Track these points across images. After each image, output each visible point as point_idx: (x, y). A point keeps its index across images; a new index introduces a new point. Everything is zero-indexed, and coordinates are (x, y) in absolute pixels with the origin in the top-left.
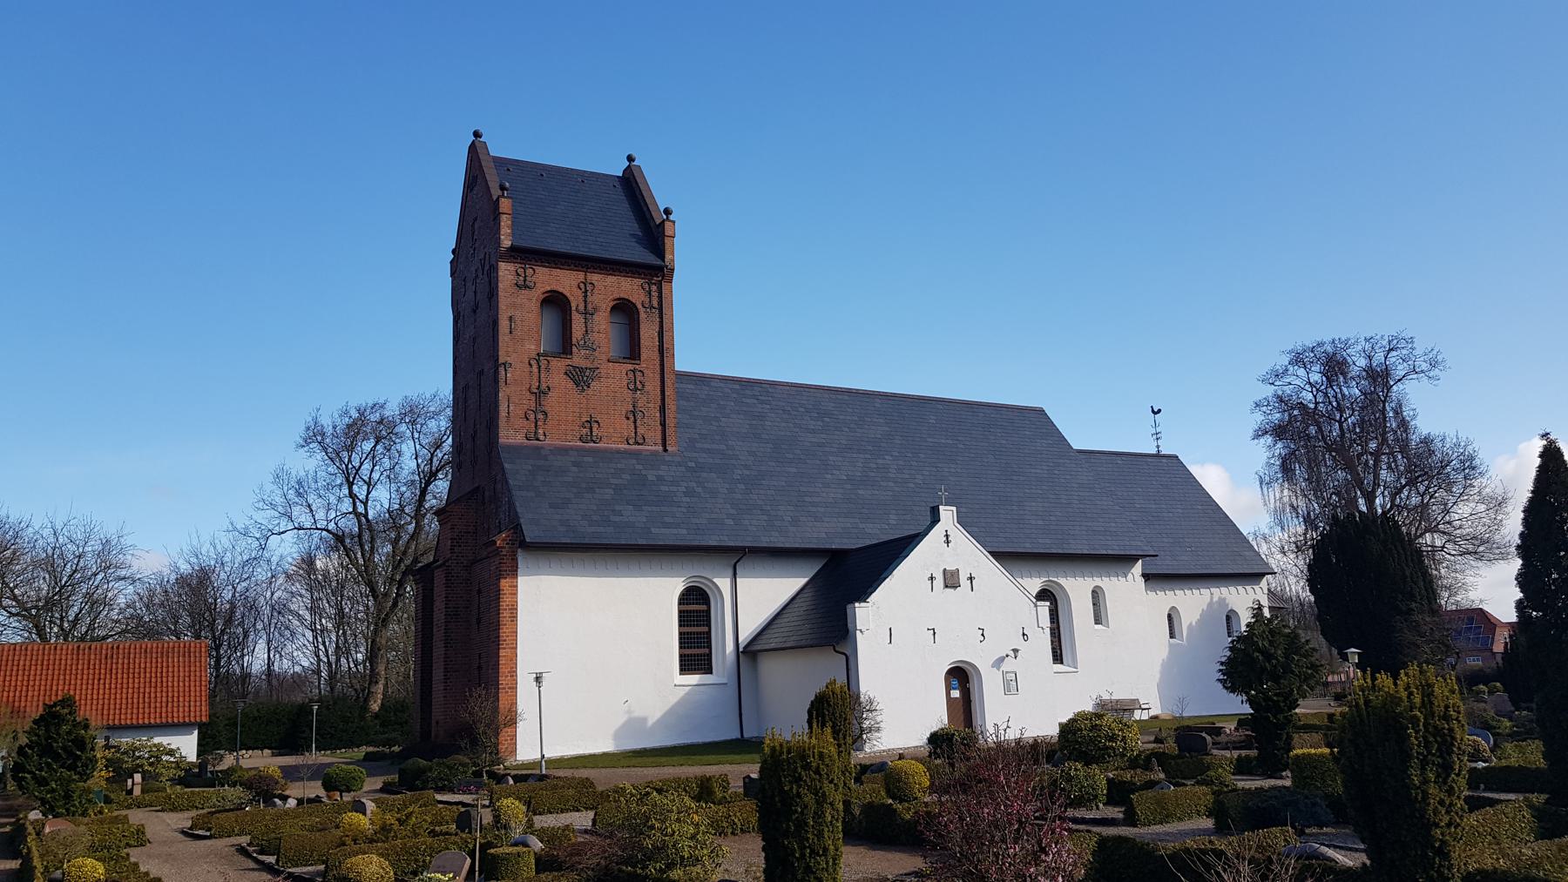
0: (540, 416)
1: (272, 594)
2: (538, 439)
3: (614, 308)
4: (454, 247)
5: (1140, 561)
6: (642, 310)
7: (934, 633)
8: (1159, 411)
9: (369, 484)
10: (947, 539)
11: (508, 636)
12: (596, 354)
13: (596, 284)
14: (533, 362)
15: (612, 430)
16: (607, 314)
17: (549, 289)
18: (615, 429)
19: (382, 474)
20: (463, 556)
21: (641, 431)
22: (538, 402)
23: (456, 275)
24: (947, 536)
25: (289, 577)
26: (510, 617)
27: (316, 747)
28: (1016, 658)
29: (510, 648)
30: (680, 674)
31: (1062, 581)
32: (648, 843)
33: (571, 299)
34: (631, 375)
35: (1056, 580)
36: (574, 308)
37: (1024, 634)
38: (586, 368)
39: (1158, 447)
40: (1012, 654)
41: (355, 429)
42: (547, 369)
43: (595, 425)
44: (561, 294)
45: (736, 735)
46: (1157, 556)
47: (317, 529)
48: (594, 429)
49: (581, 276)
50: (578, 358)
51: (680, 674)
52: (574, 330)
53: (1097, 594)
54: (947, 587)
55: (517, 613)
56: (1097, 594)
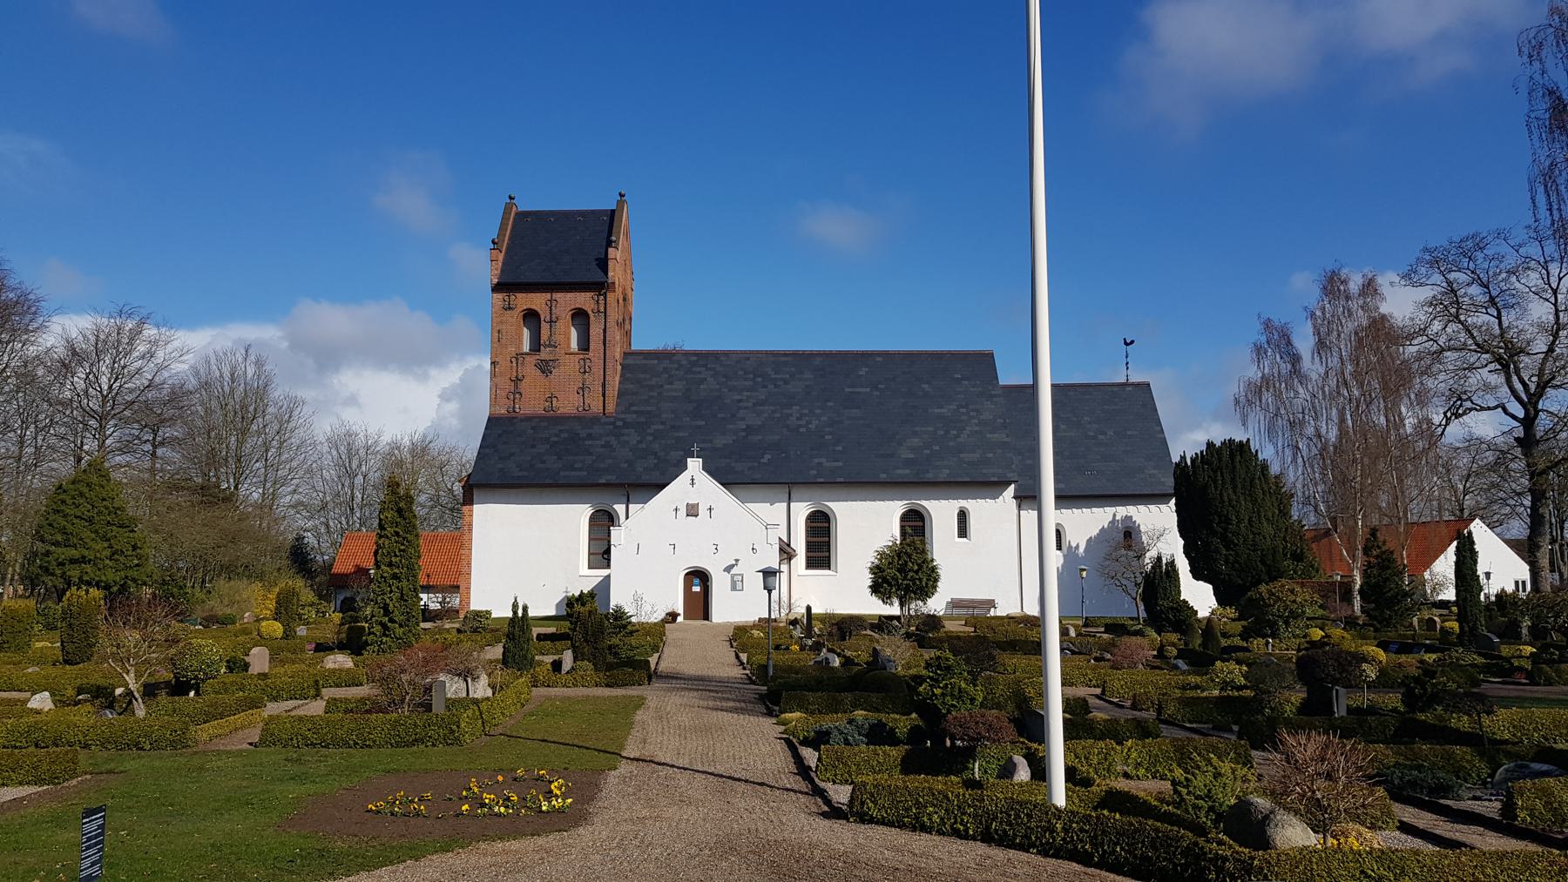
0: (517, 396)
3: (573, 316)
5: (1013, 485)
8: (1132, 342)
13: (558, 300)
14: (513, 360)
18: (569, 401)
22: (516, 386)
24: (693, 480)
31: (924, 503)
33: (540, 312)
34: (582, 362)
35: (918, 502)
36: (542, 319)
37: (753, 549)
42: (523, 364)
43: (554, 399)
44: (534, 310)
49: (548, 296)
50: (545, 354)
53: (963, 516)
54: (688, 515)
56: (963, 516)
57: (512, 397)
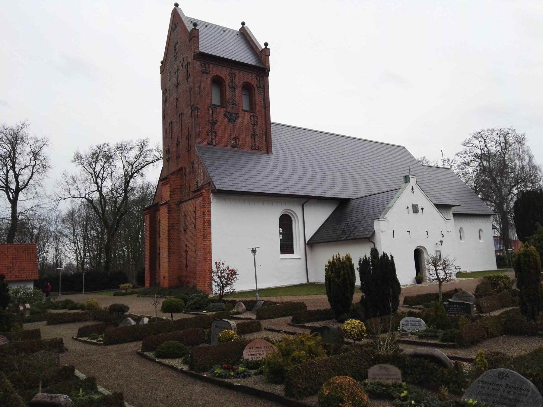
1: (57, 227)
2: (212, 145)
4: (162, 60)
6: (256, 89)
7: (410, 233)
9: (102, 180)
10: (413, 190)
11: (207, 235)
12: (237, 107)
14: (210, 108)
15: (244, 143)
16: (240, 89)
17: (216, 75)
19: (108, 175)
20: (175, 200)
21: (257, 144)
23: (164, 72)
24: (413, 189)
25: (63, 221)
26: (208, 226)
27: (84, 290)
28: (442, 245)
29: (208, 241)
30: (281, 254)
32: (319, 337)
34: (252, 118)
36: (227, 85)
37: (442, 234)
38: (233, 113)
39: (444, 164)
40: (440, 243)
41: (95, 156)
42: (216, 112)
45: (305, 281)
46: (460, 206)
47: (81, 197)
48: (237, 142)
51: (281, 254)
52: (227, 95)
55: (211, 224)
57: (210, 134)
